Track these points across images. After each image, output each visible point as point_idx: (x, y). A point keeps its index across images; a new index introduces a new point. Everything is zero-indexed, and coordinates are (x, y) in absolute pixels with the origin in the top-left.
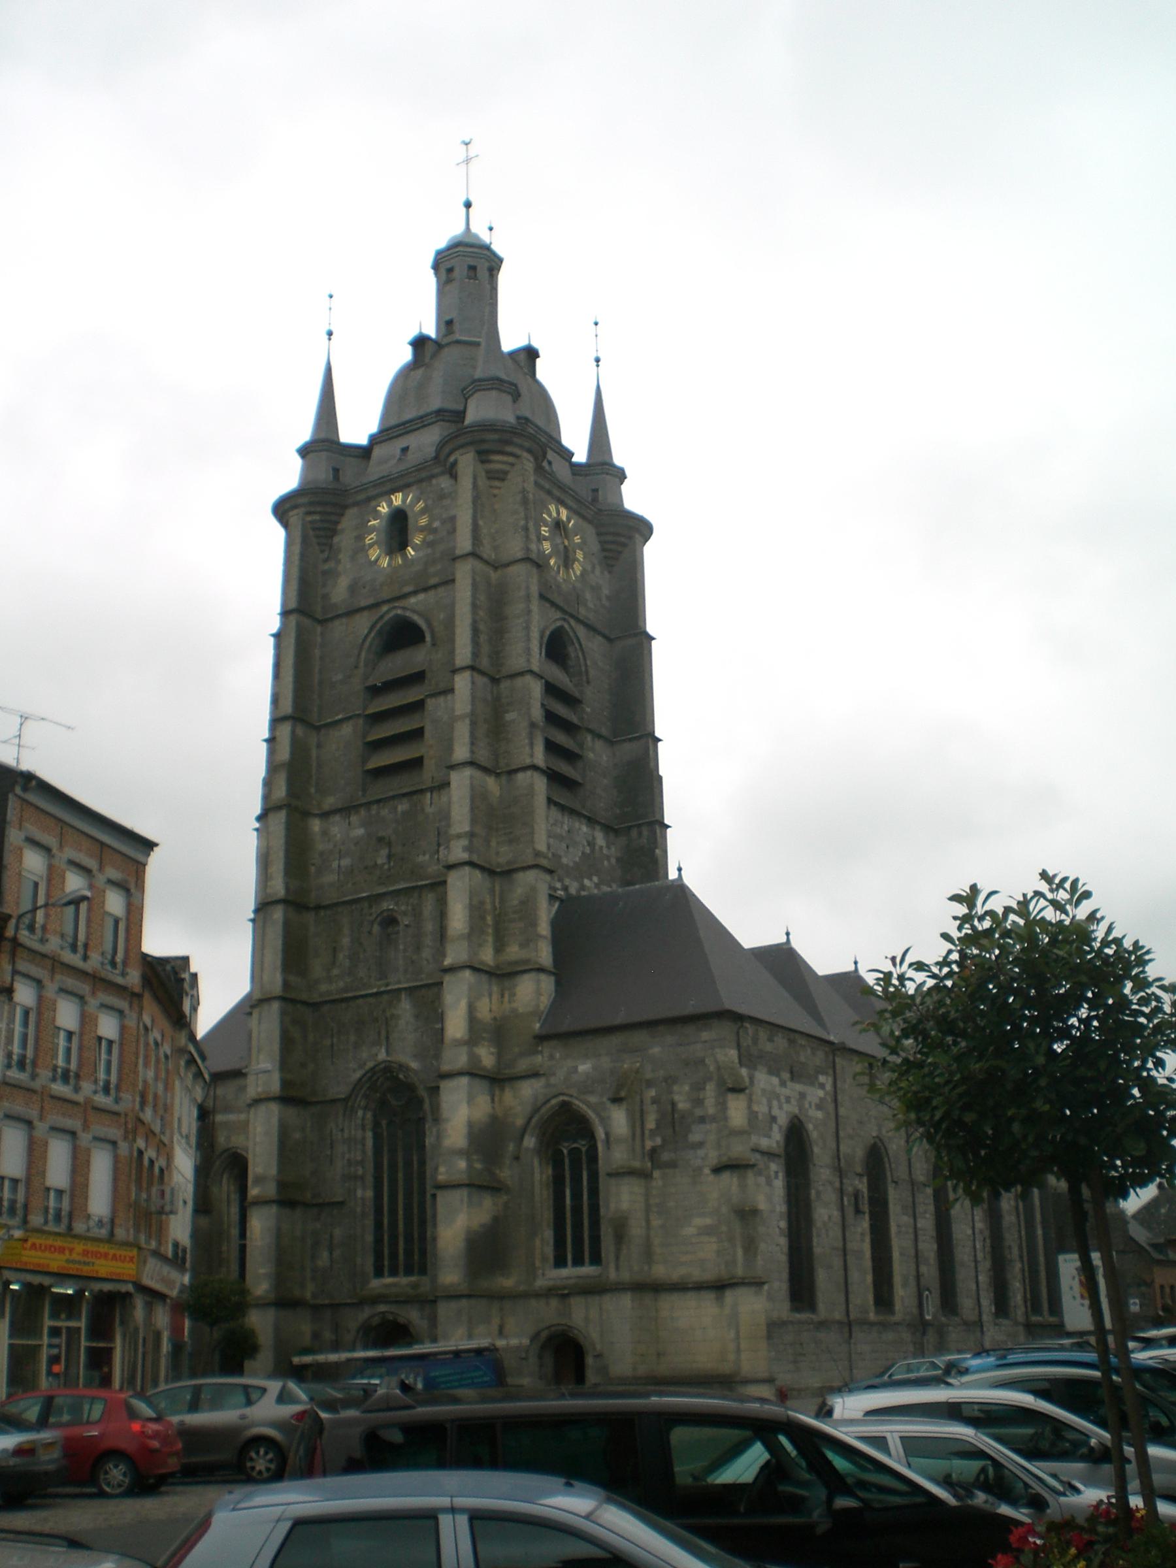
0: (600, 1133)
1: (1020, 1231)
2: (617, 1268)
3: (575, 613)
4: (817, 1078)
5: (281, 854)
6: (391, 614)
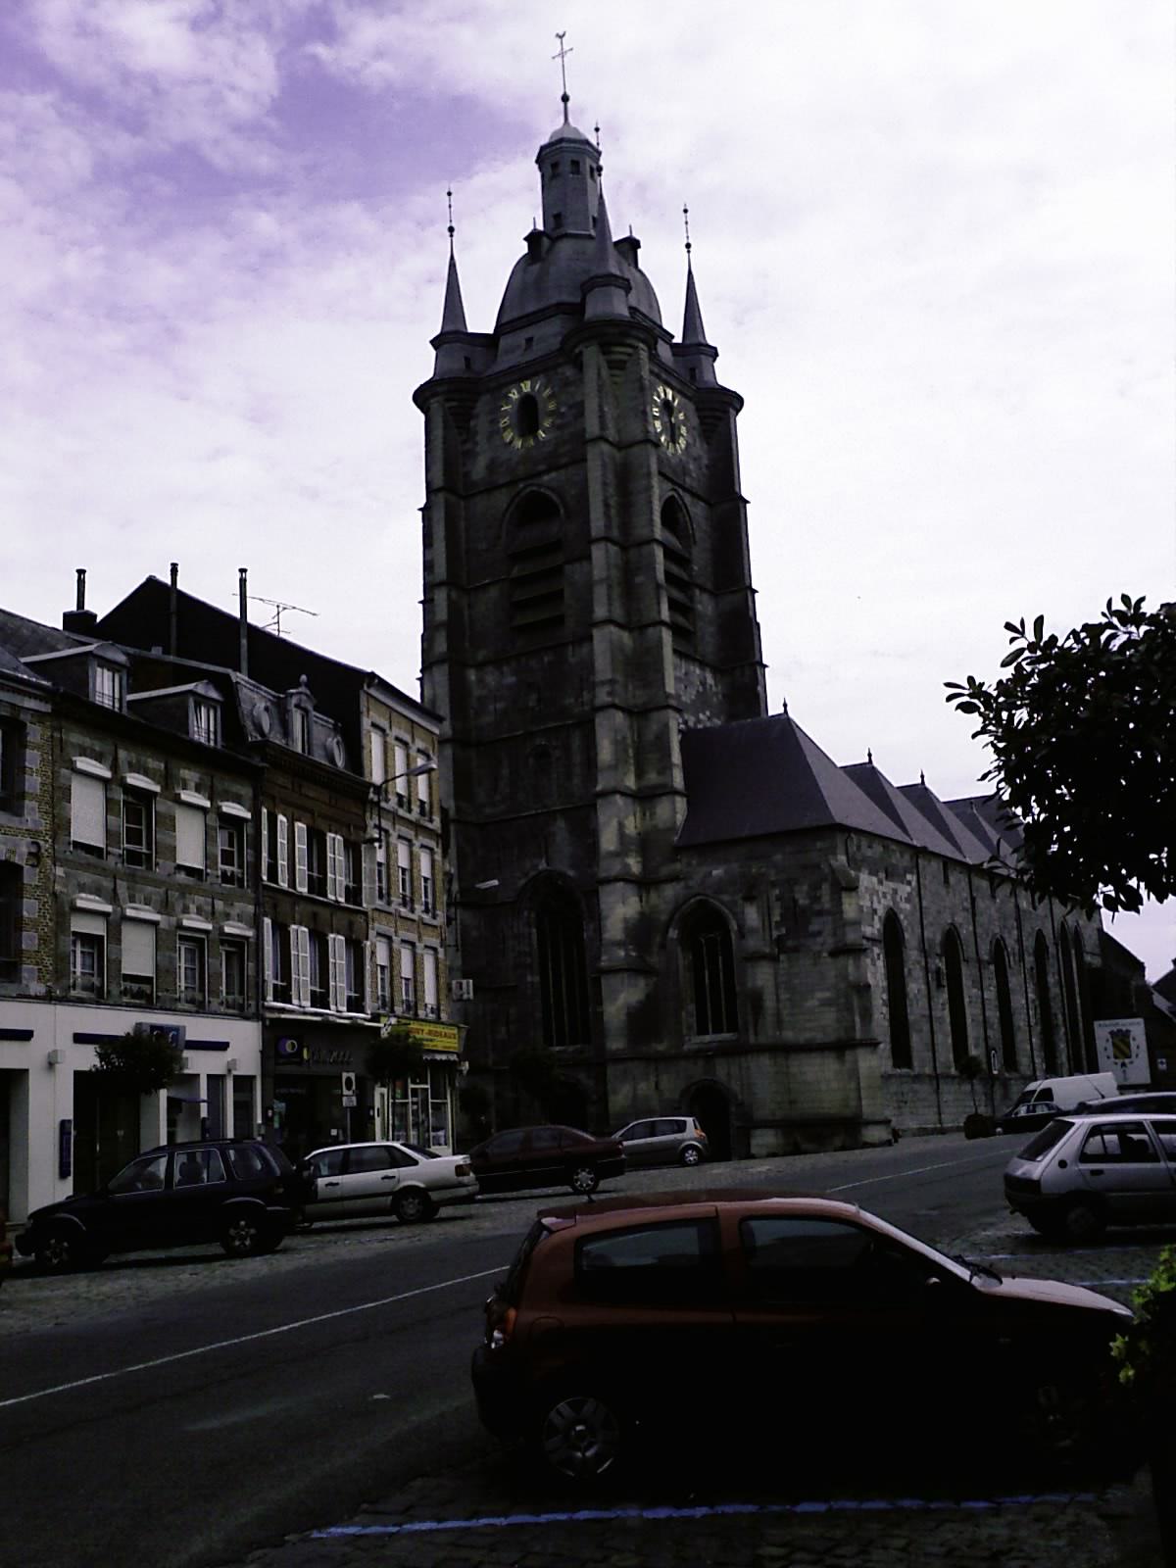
0: (734, 926)
1: (1063, 1001)
2: (756, 1034)
3: (681, 482)
4: (905, 877)
5: (447, 700)
6: (528, 490)
